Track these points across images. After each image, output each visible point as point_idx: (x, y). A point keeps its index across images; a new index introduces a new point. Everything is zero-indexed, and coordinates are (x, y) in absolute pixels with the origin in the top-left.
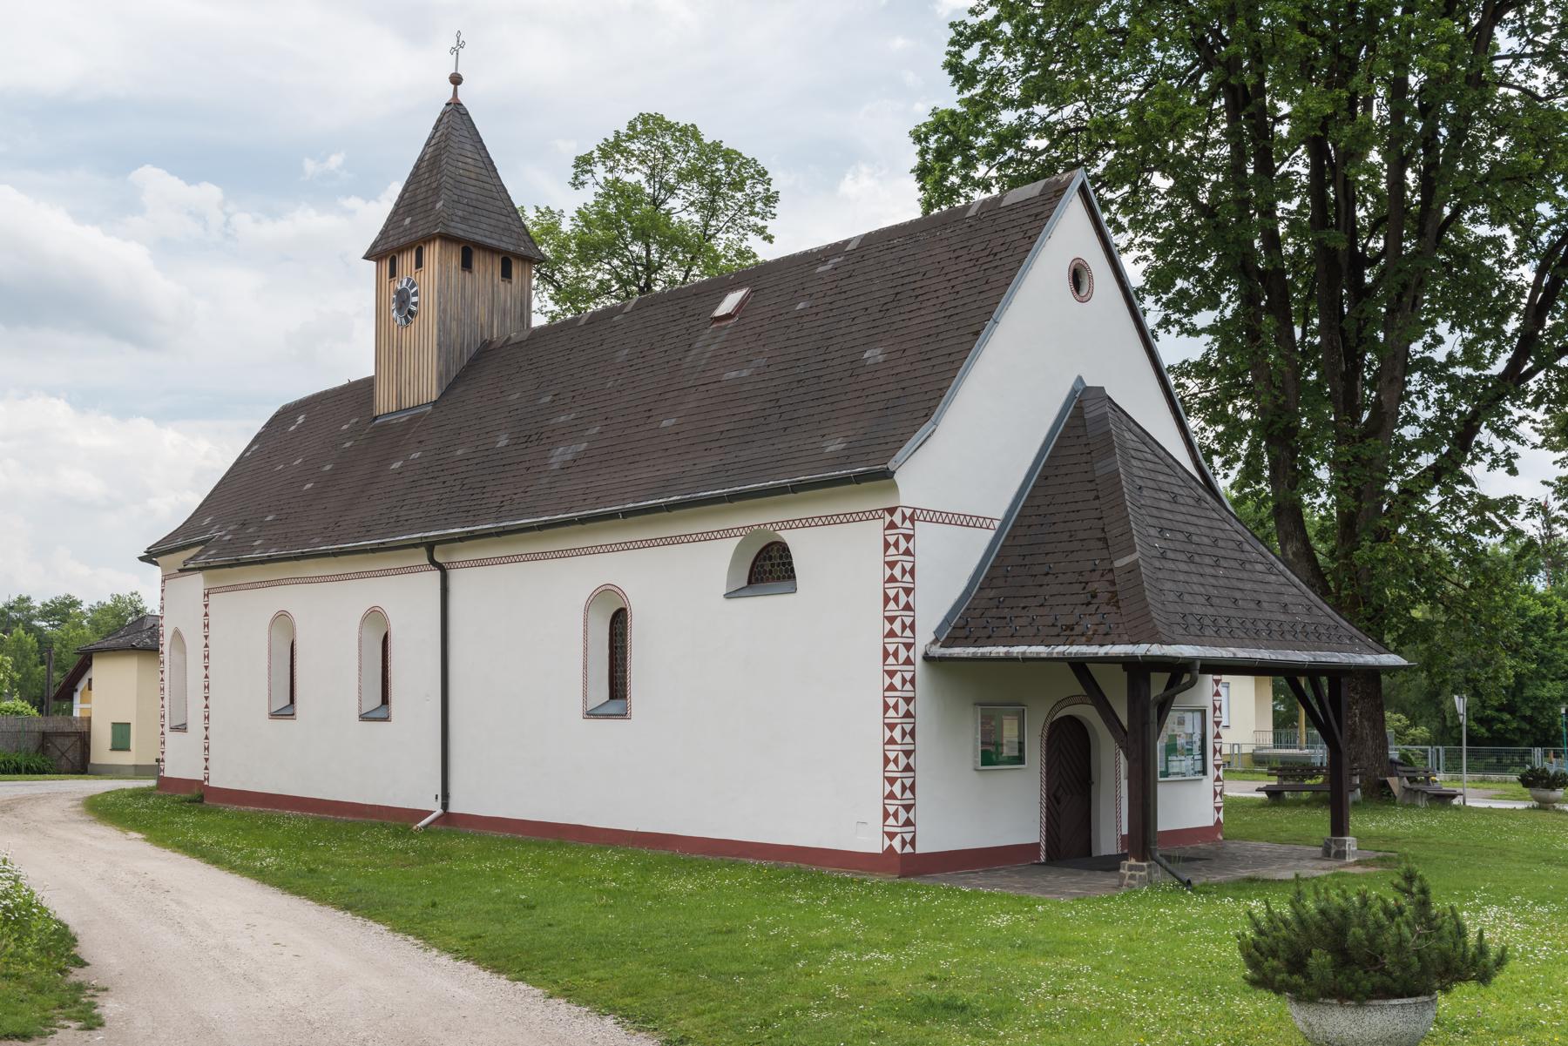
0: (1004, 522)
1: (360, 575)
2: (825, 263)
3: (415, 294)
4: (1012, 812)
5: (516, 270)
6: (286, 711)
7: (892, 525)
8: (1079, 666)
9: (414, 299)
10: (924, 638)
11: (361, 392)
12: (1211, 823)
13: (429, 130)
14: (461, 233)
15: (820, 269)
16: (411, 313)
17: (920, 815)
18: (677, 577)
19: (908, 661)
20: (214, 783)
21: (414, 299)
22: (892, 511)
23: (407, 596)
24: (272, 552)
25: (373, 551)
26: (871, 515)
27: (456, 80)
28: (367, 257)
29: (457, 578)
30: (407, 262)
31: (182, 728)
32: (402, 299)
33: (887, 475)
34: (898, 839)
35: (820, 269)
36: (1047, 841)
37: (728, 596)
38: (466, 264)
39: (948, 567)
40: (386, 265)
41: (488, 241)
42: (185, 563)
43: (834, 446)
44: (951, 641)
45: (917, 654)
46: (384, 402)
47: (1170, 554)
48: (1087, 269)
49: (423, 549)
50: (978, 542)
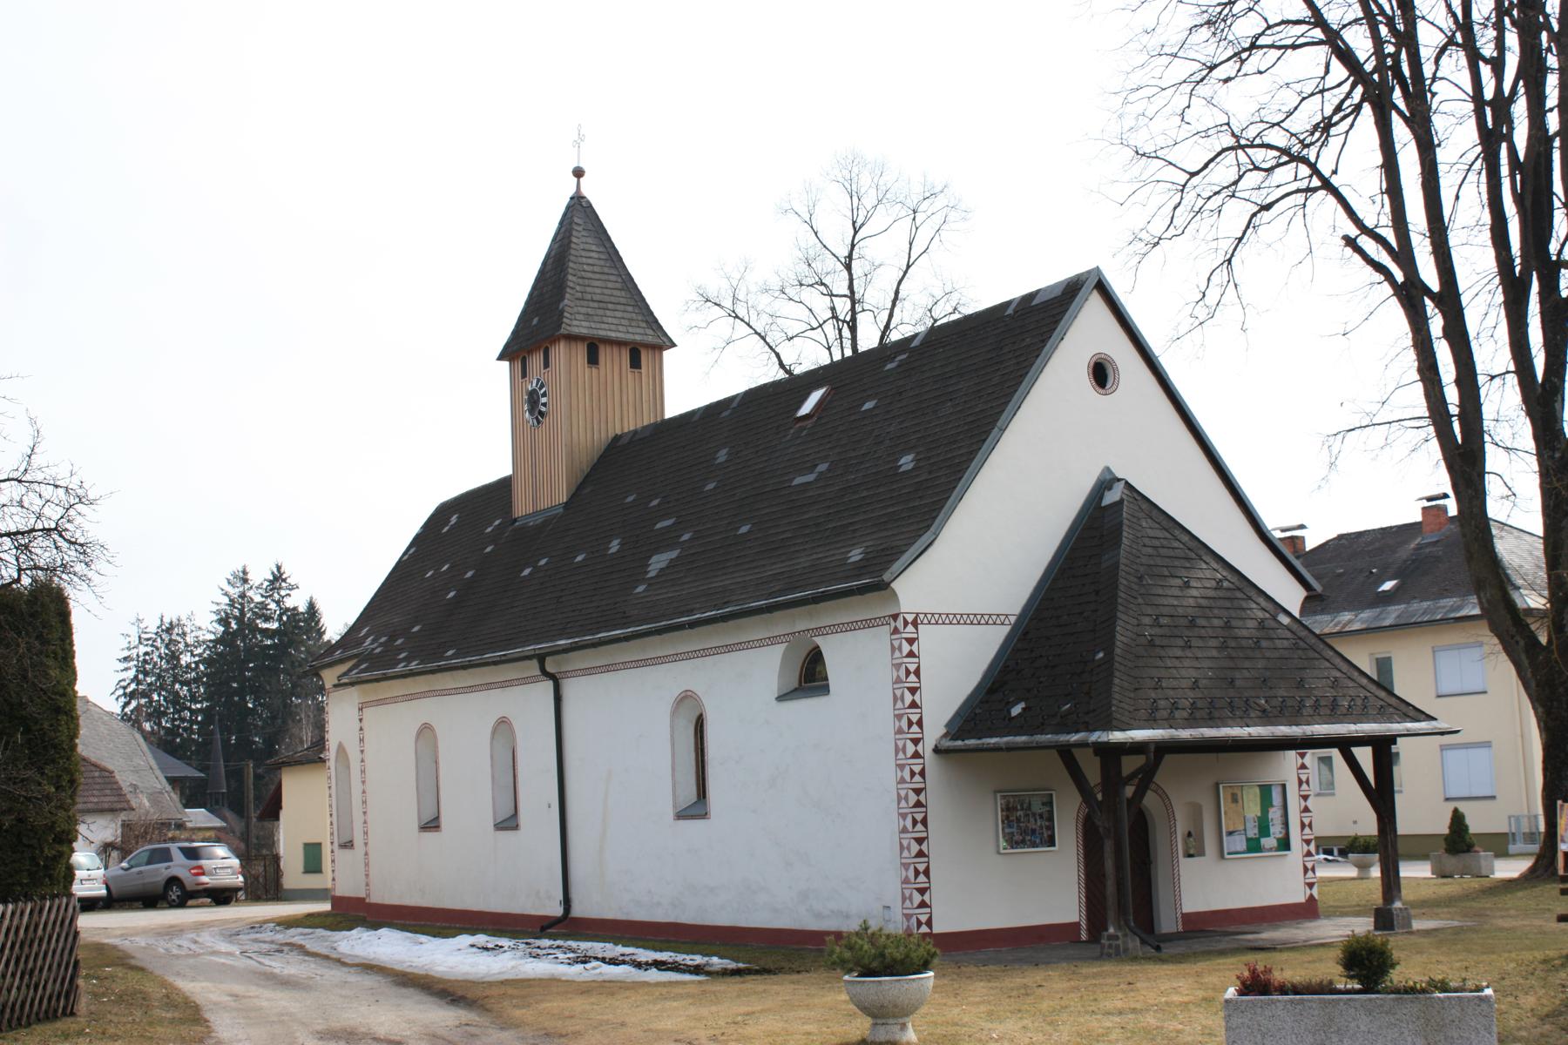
0: (1021, 617)
1: (488, 686)
2: (892, 360)
3: (544, 395)
4: (1050, 888)
5: (645, 357)
6: (697, 807)
7: (896, 631)
8: (1066, 752)
9: (544, 400)
10: (934, 731)
11: (498, 493)
12: (1302, 900)
13: (556, 225)
14: (584, 331)
15: (889, 366)
16: (541, 413)
17: (936, 897)
18: (737, 679)
19: (916, 755)
20: (375, 899)
21: (544, 400)
22: (895, 617)
23: (528, 704)
24: (413, 665)
25: (495, 663)
26: (868, 624)
27: (578, 173)
28: (501, 357)
29: (571, 688)
30: (536, 361)
31: (348, 845)
32: (533, 399)
33: (883, 586)
34: (914, 920)
35: (889, 366)
36: (1089, 919)
37: (782, 698)
38: (593, 360)
39: (955, 666)
40: (518, 365)
41: (613, 334)
42: (339, 678)
43: (856, 555)
44: (954, 738)
45: (927, 747)
46: (523, 506)
47: (1157, 642)
48: (1112, 362)
49: (535, 663)
50: (992, 640)
